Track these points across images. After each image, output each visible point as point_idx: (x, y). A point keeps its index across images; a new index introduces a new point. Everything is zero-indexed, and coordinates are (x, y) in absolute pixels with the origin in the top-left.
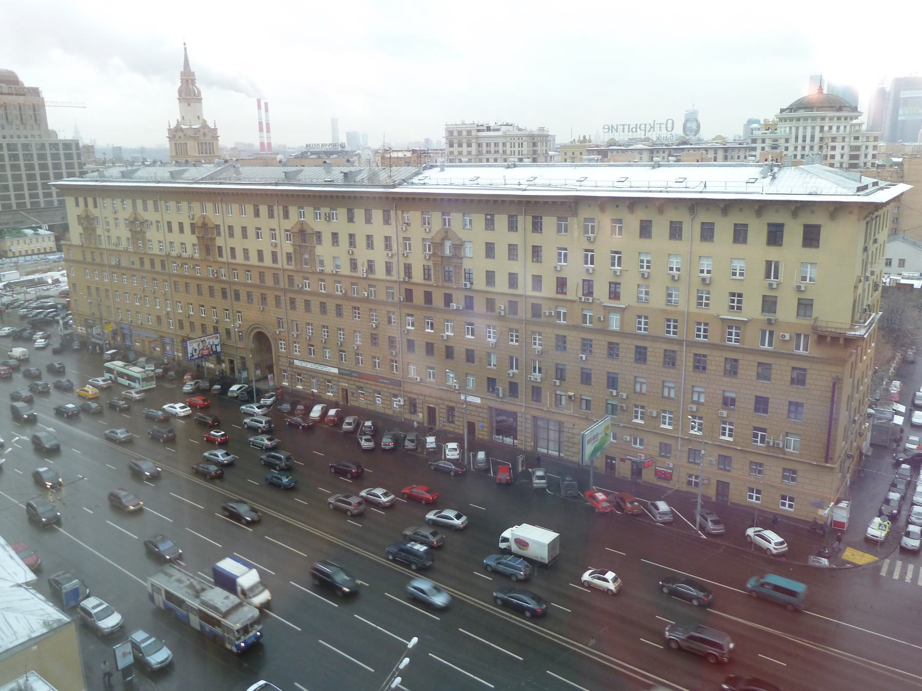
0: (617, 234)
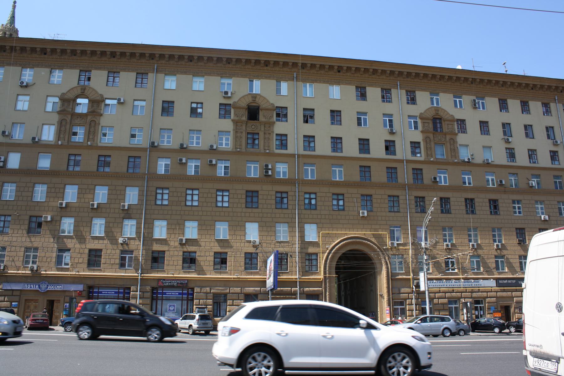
0: (26, 73)
